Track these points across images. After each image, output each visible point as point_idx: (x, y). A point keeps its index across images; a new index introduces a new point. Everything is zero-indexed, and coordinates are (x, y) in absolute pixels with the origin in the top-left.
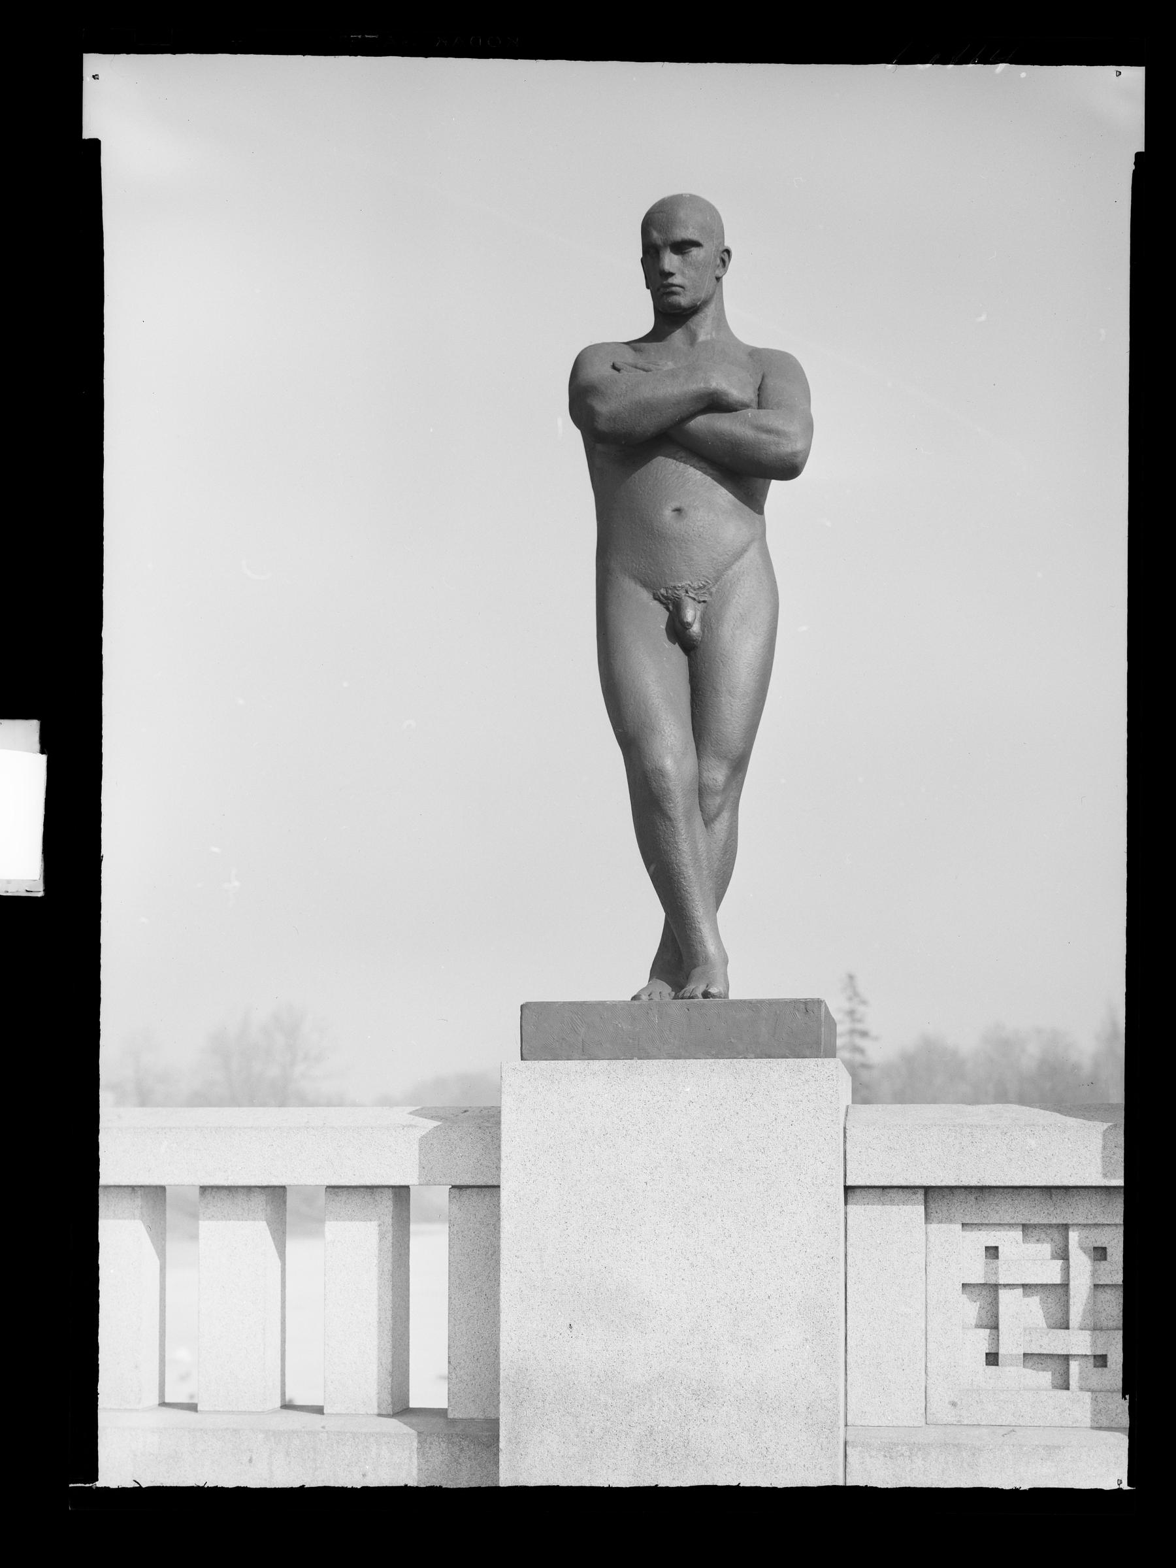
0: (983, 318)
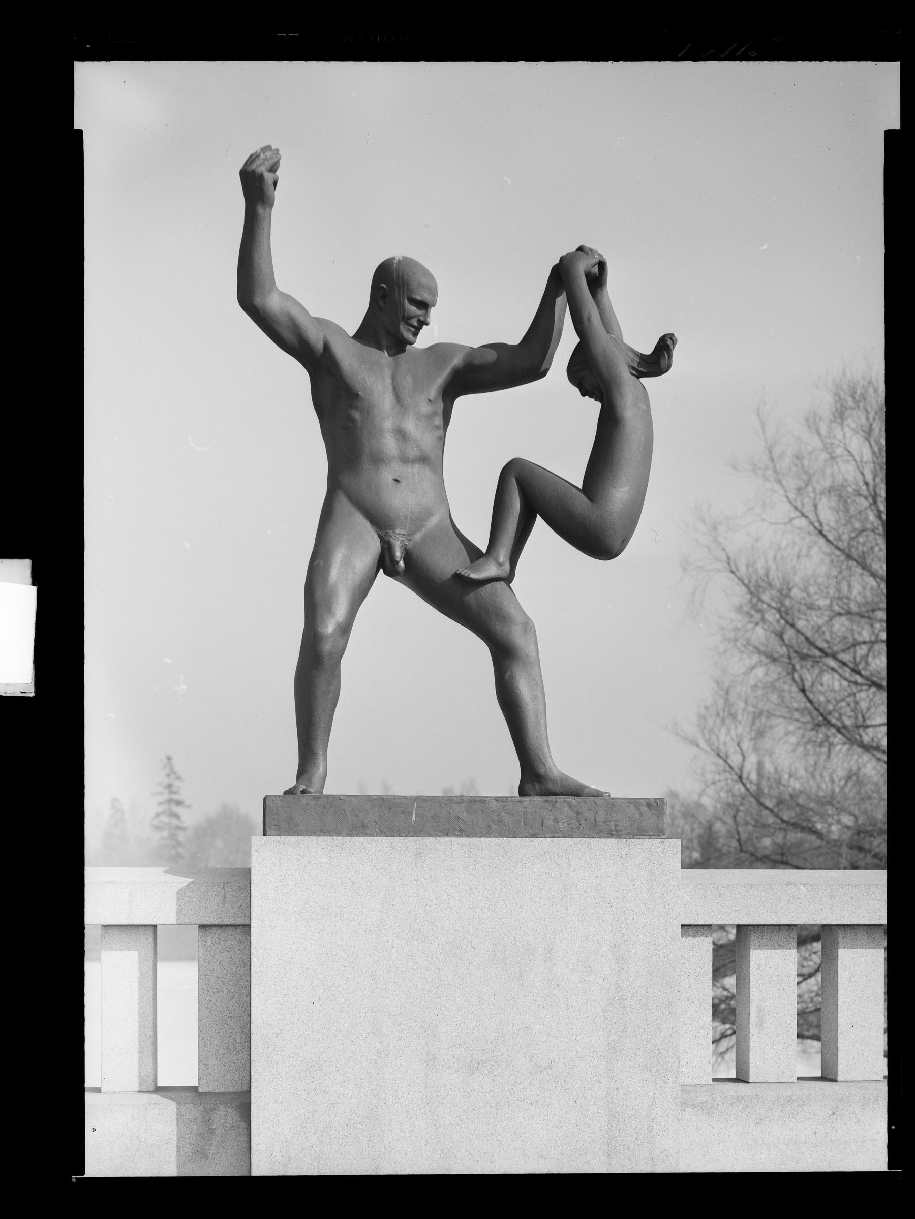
0: (765, 247)
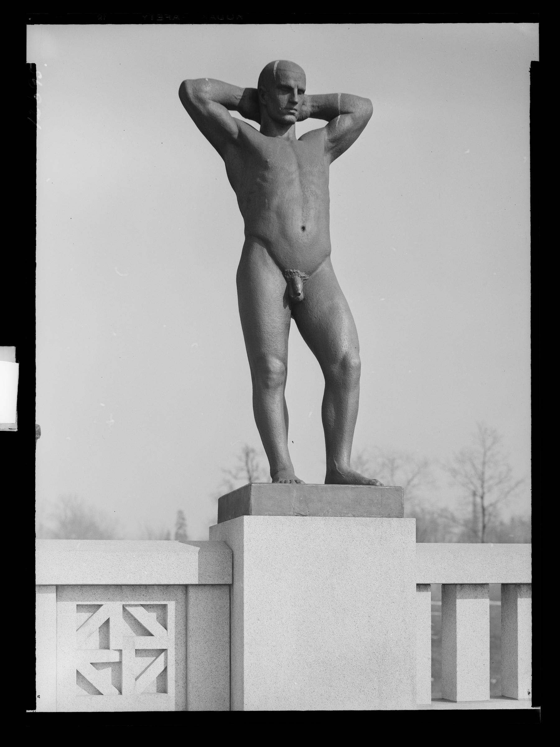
0: (468, 152)
